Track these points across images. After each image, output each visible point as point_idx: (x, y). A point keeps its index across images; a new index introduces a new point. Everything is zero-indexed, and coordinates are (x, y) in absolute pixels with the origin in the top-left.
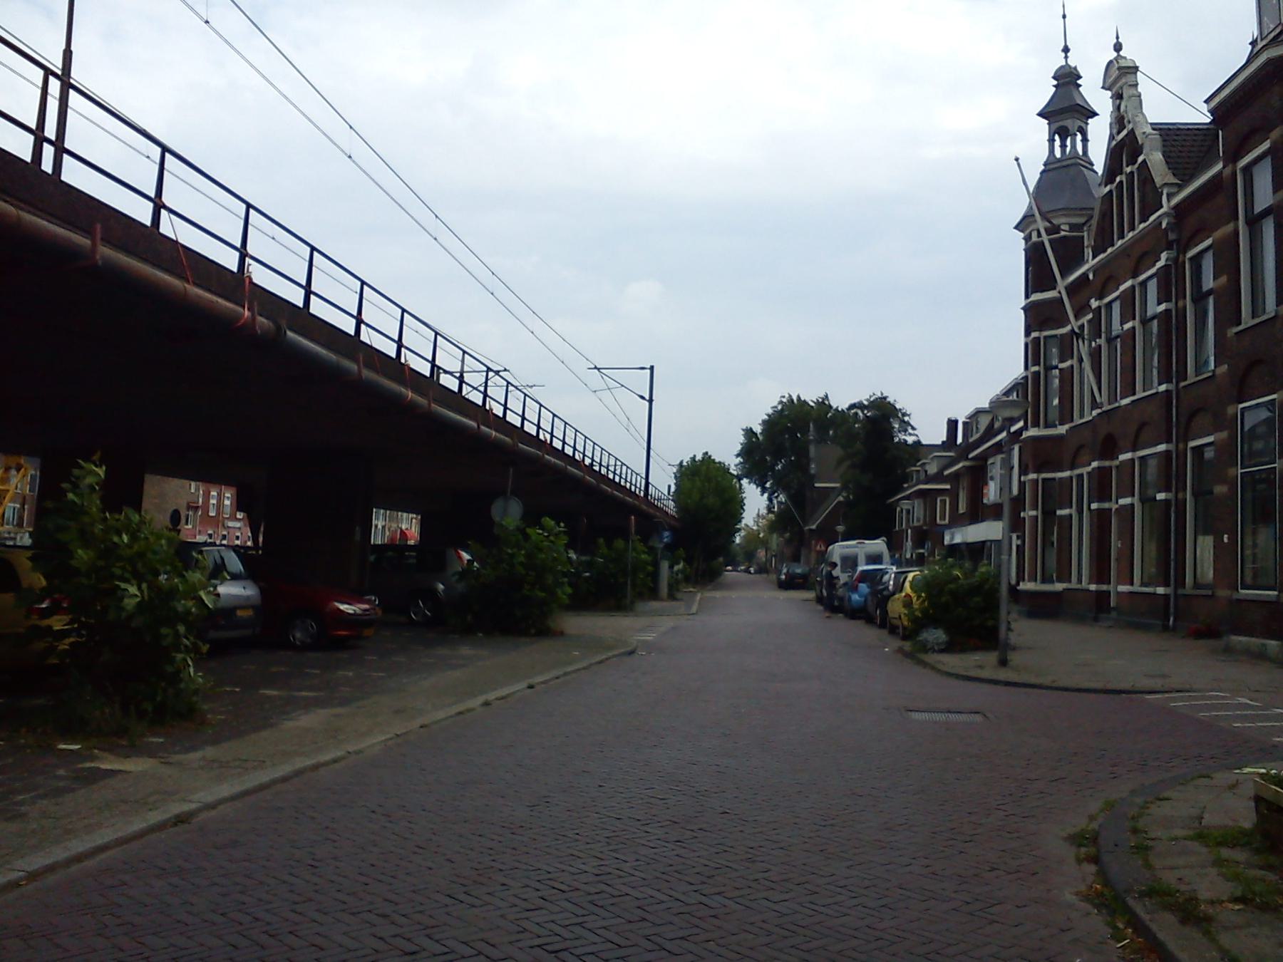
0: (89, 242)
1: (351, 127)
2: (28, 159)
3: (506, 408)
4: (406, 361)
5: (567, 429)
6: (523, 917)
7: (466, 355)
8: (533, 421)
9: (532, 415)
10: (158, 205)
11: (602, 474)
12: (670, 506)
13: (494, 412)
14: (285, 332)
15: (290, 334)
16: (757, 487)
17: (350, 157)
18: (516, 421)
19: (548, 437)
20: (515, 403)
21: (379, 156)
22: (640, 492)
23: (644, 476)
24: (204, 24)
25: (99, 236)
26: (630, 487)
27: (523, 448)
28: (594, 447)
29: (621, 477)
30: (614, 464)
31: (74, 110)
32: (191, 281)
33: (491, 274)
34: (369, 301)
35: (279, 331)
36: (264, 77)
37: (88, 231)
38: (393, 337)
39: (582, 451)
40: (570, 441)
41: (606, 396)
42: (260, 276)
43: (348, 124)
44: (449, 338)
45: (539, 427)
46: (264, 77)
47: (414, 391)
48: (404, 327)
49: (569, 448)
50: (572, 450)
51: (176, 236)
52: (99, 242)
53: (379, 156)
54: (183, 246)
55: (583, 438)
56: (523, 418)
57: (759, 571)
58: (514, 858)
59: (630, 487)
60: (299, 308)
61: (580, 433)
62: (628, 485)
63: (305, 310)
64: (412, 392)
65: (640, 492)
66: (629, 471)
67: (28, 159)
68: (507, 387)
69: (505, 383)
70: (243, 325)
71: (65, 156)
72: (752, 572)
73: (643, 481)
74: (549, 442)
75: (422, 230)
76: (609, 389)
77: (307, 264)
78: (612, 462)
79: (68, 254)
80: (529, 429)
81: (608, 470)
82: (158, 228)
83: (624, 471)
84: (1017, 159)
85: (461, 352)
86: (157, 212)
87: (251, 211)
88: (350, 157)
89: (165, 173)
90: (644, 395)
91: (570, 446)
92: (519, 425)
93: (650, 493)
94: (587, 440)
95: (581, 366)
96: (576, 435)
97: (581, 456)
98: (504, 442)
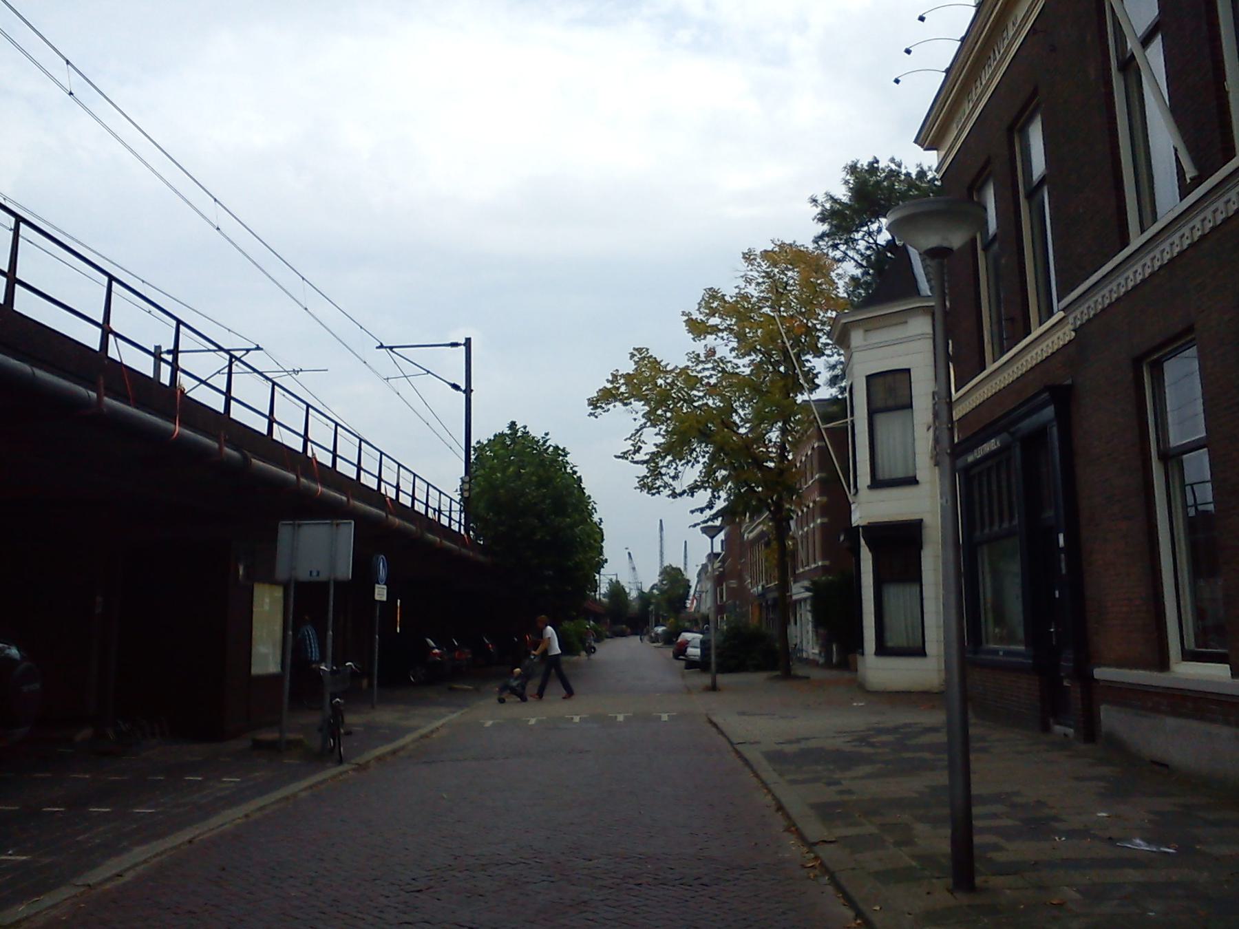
1: (215, 200)
4: (313, 454)
7: (401, 468)
10: (106, 330)
12: (453, 518)
14: (251, 461)
15: (253, 460)
18: (372, 483)
20: (347, 448)
21: (230, 213)
25: (299, 473)
31: (25, 239)
33: (213, 200)
35: (246, 459)
37: (91, 384)
40: (421, 496)
43: (213, 197)
45: (414, 498)
47: (323, 484)
50: (447, 519)
52: (300, 476)
53: (230, 213)
56: (359, 469)
60: (220, 413)
63: (269, 437)
64: (321, 486)
71: (17, 286)
74: (437, 520)
76: (405, 376)
79: (201, 453)
82: (12, 305)
87: (114, 283)
88: (218, 229)
92: (409, 505)
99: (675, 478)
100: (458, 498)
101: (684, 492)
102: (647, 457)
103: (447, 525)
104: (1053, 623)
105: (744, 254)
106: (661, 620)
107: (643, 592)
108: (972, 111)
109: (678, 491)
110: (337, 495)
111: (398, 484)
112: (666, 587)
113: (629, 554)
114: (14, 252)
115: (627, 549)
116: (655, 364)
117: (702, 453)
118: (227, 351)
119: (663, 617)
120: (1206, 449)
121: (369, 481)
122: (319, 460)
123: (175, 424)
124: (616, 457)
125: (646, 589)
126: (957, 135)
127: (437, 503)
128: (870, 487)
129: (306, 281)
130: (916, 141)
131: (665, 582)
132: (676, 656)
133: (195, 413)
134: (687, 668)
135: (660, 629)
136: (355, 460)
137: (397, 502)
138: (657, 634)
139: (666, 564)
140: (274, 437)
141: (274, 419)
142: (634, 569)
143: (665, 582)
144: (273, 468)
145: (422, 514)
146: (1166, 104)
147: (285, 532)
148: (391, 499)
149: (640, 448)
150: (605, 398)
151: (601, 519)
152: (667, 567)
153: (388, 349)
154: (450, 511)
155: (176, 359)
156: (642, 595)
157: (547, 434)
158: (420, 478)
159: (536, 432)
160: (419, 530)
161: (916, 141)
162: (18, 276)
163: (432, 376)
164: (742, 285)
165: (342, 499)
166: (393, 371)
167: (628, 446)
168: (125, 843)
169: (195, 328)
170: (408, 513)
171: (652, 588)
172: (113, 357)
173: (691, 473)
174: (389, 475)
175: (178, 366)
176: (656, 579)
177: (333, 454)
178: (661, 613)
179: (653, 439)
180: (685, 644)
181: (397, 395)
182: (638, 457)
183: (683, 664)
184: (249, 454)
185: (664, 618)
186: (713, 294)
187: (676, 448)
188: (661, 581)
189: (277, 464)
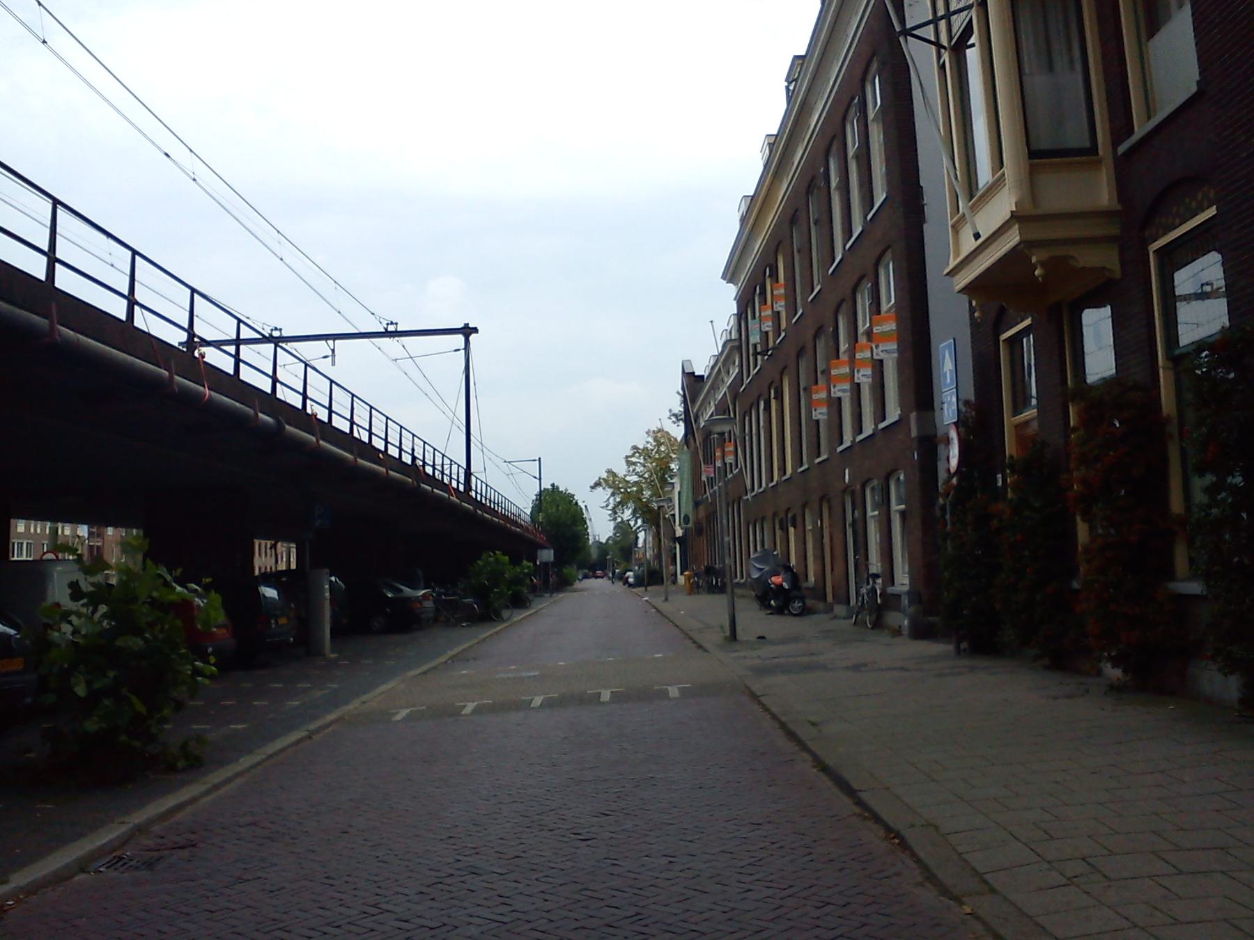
0: (167, 373)
1: (191, 151)
3: (331, 411)
4: (312, 410)
5: (355, 403)
6: (447, 886)
8: (345, 416)
9: (378, 429)
13: (318, 417)
15: (287, 427)
17: (281, 259)
18: (344, 426)
19: (421, 463)
23: (464, 466)
30: (441, 463)
32: (206, 386)
35: (280, 427)
36: (140, 131)
38: (298, 389)
40: (394, 438)
41: (511, 476)
44: (225, 307)
45: (401, 450)
46: (140, 131)
49: (407, 455)
56: (352, 423)
57: (640, 582)
59: (502, 511)
61: (429, 445)
62: (461, 488)
68: (451, 465)
71: (57, 265)
72: (631, 580)
73: (462, 471)
75: (262, 245)
76: (411, 358)
77: (48, 231)
78: (447, 461)
81: (451, 478)
84: (712, 322)
86: (51, 266)
87: (137, 257)
91: (365, 429)
93: (474, 488)
94: (355, 398)
97: (449, 478)
98: (470, 509)
104: (385, 591)
106: (615, 565)
107: (601, 543)
108: (749, 263)
111: (413, 450)
112: (619, 539)
114: (53, 239)
115: (584, 502)
116: (614, 475)
117: (631, 505)
119: (617, 562)
120: (946, 423)
121: (341, 424)
123: (204, 387)
126: (743, 277)
129: (195, 154)
130: (724, 277)
131: (618, 535)
132: (624, 584)
141: (135, 299)
143: (618, 535)
146: (940, 133)
147: (12, 521)
148: (453, 488)
150: (597, 484)
158: (429, 445)
160: (415, 483)
161: (724, 277)
162: (58, 255)
163: (538, 484)
164: (645, 443)
166: (508, 472)
167: (605, 504)
169: (161, 265)
170: (327, 429)
174: (361, 417)
175: (193, 331)
177: (189, 334)
178: (615, 559)
180: (628, 577)
181: (405, 375)
186: (635, 447)
188: (615, 534)
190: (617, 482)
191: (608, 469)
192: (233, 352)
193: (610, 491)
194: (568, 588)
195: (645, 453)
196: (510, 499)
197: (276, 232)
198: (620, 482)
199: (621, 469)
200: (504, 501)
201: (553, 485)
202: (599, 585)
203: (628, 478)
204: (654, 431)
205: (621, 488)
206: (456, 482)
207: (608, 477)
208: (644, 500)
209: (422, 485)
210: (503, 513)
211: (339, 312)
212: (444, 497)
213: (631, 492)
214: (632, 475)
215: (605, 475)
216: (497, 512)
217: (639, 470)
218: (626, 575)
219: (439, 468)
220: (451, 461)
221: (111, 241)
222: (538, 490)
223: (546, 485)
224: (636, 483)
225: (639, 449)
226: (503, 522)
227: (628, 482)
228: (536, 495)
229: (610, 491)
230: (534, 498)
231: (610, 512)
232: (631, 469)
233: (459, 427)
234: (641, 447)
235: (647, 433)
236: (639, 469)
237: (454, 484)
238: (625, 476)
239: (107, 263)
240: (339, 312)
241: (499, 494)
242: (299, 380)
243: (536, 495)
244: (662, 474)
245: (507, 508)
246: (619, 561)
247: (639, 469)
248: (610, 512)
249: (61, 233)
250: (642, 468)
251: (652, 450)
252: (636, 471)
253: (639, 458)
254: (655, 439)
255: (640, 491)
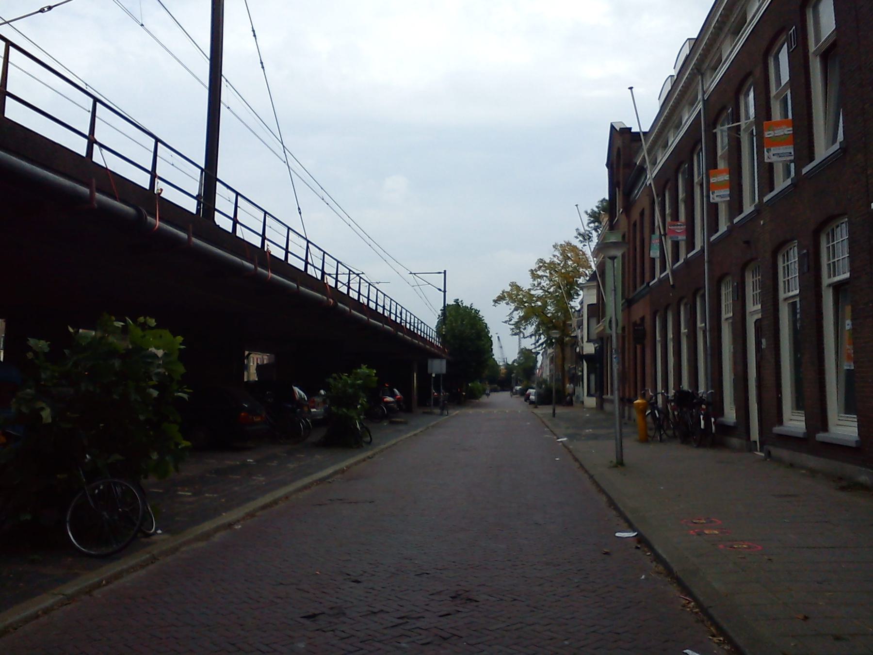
2: (148, 187)
4: (268, 249)
11: (385, 316)
14: (146, 217)
16: (518, 319)
20: (316, 258)
22: (417, 331)
24: (140, 27)
25: (94, 186)
26: (424, 336)
27: (357, 316)
28: (308, 247)
29: (410, 325)
34: (149, 150)
35: (336, 305)
38: (259, 233)
39: (389, 310)
40: (364, 291)
42: (169, 194)
45: (369, 299)
48: (290, 242)
51: (106, 165)
53: (246, 102)
54: (330, 286)
55: (390, 300)
58: (372, 569)
59: (424, 336)
65: (417, 331)
66: (408, 314)
67: (148, 187)
68: (349, 274)
69: (348, 271)
70: (159, 226)
71: (7, 97)
72: (532, 397)
76: (419, 286)
77: (152, 155)
78: (420, 322)
79: (284, 288)
80: (275, 253)
82: (287, 261)
83: (412, 321)
84: (631, 88)
85: (91, 100)
89: (158, 158)
90: (440, 288)
94: (392, 301)
95: (406, 274)
96: (308, 247)
97: (388, 313)
99: (525, 329)
100: (435, 330)
101: (528, 337)
102: (514, 323)
103: (382, 312)
105: (553, 246)
106: (519, 382)
107: (508, 364)
109: (525, 336)
110: (239, 260)
113: (498, 337)
115: (497, 334)
116: (518, 288)
117: (535, 321)
118: (358, 275)
119: (520, 380)
122: (272, 253)
123: (156, 219)
124: (503, 322)
125: (510, 363)
127: (383, 303)
128: (587, 342)
132: (526, 400)
133: (243, 247)
134: (530, 404)
135: (518, 388)
136: (231, 214)
137: (305, 272)
138: (516, 390)
139: (522, 347)
140: (237, 235)
142: (501, 347)
143: (521, 358)
144: (14, 158)
145: (355, 300)
147: (430, 362)
149: (512, 319)
150: (500, 298)
151: (492, 336)
152: (523, 349)
153: (414, 275)
154: (337, 274)
155: (337, 277)
156: (507, 365)
157: (472, 304)
159: (466, 303)
164: (552, 257)
165: (345, 309)
166: (413, 283)
167: (507, 319)
168: (259, 475)
170: (282, 266)
171: (514, 362)
172: (310, 274)
173: (531, 329)
176: (515, 356)
178: (519, 378)
179: (517, 316)
182: (510, 323)
183: (528, 403)
184: (144, 211)
185: (520, 380)
186: (541, 261)
187: (525, 319)
188: (519, 358)
189: (312, 289)
190: (521, 296)
191: (512, 283)
192: (342, 285)
193: (513, 306)
194: (473, 400)
195: (551, 267)
196: (428, 325)
197: (320, 188)
198: (524, 296)
199: (526, 283)
200: (412, 321)
201: (456, 301)
202: (502, 397)
203: (532, 292)
204: (561, 245)
205: (526, 302)
206: (394, 316)
207: (511, 290)
208: (549, 315)
209: (339, 304)
210: (431, 340)
211: (350, 225)
212: (362, 319)
213: (535, 306)
214: (537, 289)
215: (508, 289)
216: (434, 344)
217: (545, 284)
218: (528, 392)
219: (413, 324)
220: (350, 270)
221: (229, 191)
222: (443, 305)
223: (450, 301)
224: (539, 298)
225: (545, 263)
226: (422, 344)
227: (533, 296)
228: (441, 310)
229: (513, 306)
230: (440, 313)
231: (513, 327)
232: (536, 283)
233: (426, 304)
234: (548, 261)
235: (554, 246)
236: (545, 283)
237: (393, 317)
238: (530, 290)
239: (170, 163)
240: (350, 225)
241: (427, 326)
242: (231, 204)
243: (441, 310)
244: (569, 287)
245: (428, 334)
246: (521, 379)
247: (545, 283)
248: (513, 327)
249: (292, 240)
250: (548, 282)
251: (559, 264)
252: (541, 285)
253: (544, 271)
254: (563, 253)
255: (545, 305)
